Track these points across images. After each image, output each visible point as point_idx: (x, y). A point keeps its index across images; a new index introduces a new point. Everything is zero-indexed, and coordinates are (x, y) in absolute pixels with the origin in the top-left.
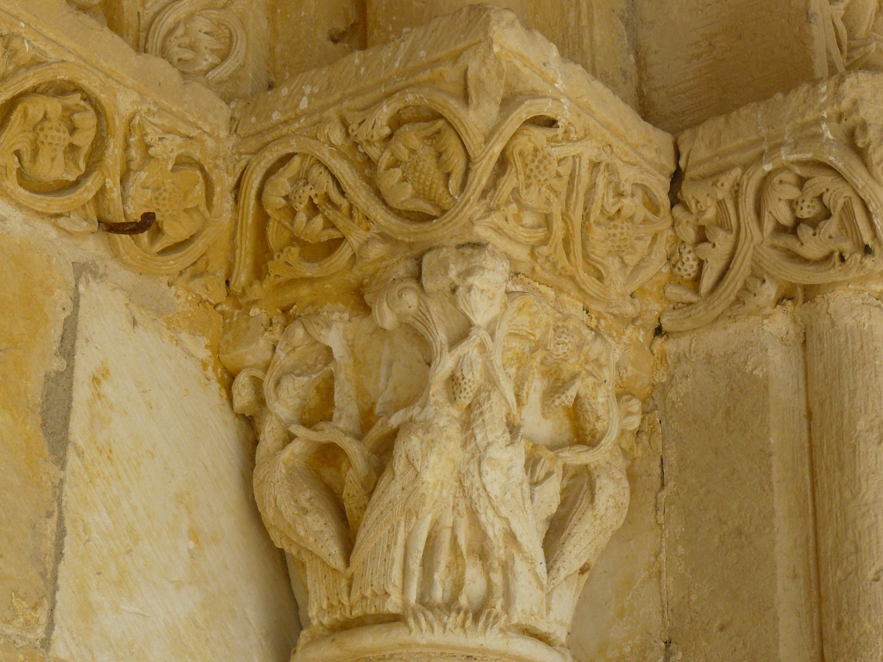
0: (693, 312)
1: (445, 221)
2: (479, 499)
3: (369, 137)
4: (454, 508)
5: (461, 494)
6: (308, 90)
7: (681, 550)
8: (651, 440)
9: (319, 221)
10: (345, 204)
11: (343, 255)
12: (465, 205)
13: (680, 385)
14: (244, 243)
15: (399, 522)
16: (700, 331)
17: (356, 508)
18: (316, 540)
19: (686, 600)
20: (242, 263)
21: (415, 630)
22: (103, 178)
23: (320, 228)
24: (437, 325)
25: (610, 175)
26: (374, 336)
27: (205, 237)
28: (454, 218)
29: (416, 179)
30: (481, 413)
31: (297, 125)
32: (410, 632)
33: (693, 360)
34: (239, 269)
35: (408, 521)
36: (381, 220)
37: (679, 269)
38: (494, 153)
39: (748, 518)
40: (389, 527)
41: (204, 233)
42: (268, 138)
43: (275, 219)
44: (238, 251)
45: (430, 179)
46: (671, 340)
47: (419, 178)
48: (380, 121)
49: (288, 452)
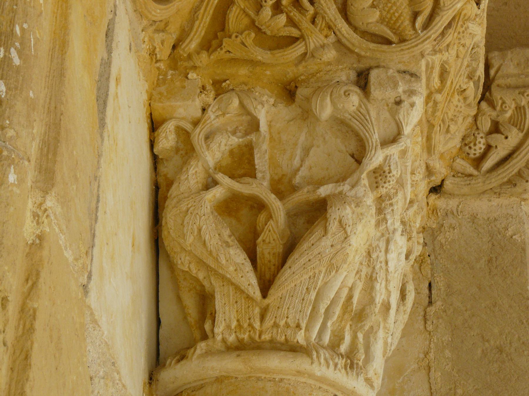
0: (473, 182)
1: (404, 48)
2: (380, 271)
4: (357, 272)
5: (366, 263)
7: (448, 353)
8: (422, 267)
9: (282, 19)
10: (311, 10)
11: (298, 49)
12: (426, 40)
13: (448, 233)
14: (205, 17)
15: (320, 272)
16: (469, 198)
17: (269, 253)
18: (236, 270)
19: (452, 392)
20: (198, 34)
21: (316, 363)
23: (283, 24)
24: (374, 126)
25: (471, 60)
26: (292, 123)
28: (413, 47)
29: (387, 9)
30: (391, 205)
32: (312, 363)
33: (460, 217)
35: (328, 272)
37: (470, 148)
38: (457, 8)
39: (508, 341)
40: (311, 274)
44: (197, 23)
45: (400, 12)
46: (443, 199)
47: (391, 8)
49: (212, 194)
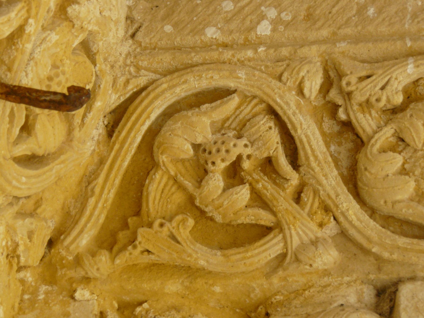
3: (373, 100)
6: (272, 13)
14: (106, 191)
20: (92, 220)
22: (26, 16)
23: (244, 203)
27: (63, 162)
31: (250, 53)
34: (85, 225)
36: (353, 217)
41: (63, 157)
42: (196, 58)
43: (168, 172)
44: (92, 201)
48: (396, 83)
